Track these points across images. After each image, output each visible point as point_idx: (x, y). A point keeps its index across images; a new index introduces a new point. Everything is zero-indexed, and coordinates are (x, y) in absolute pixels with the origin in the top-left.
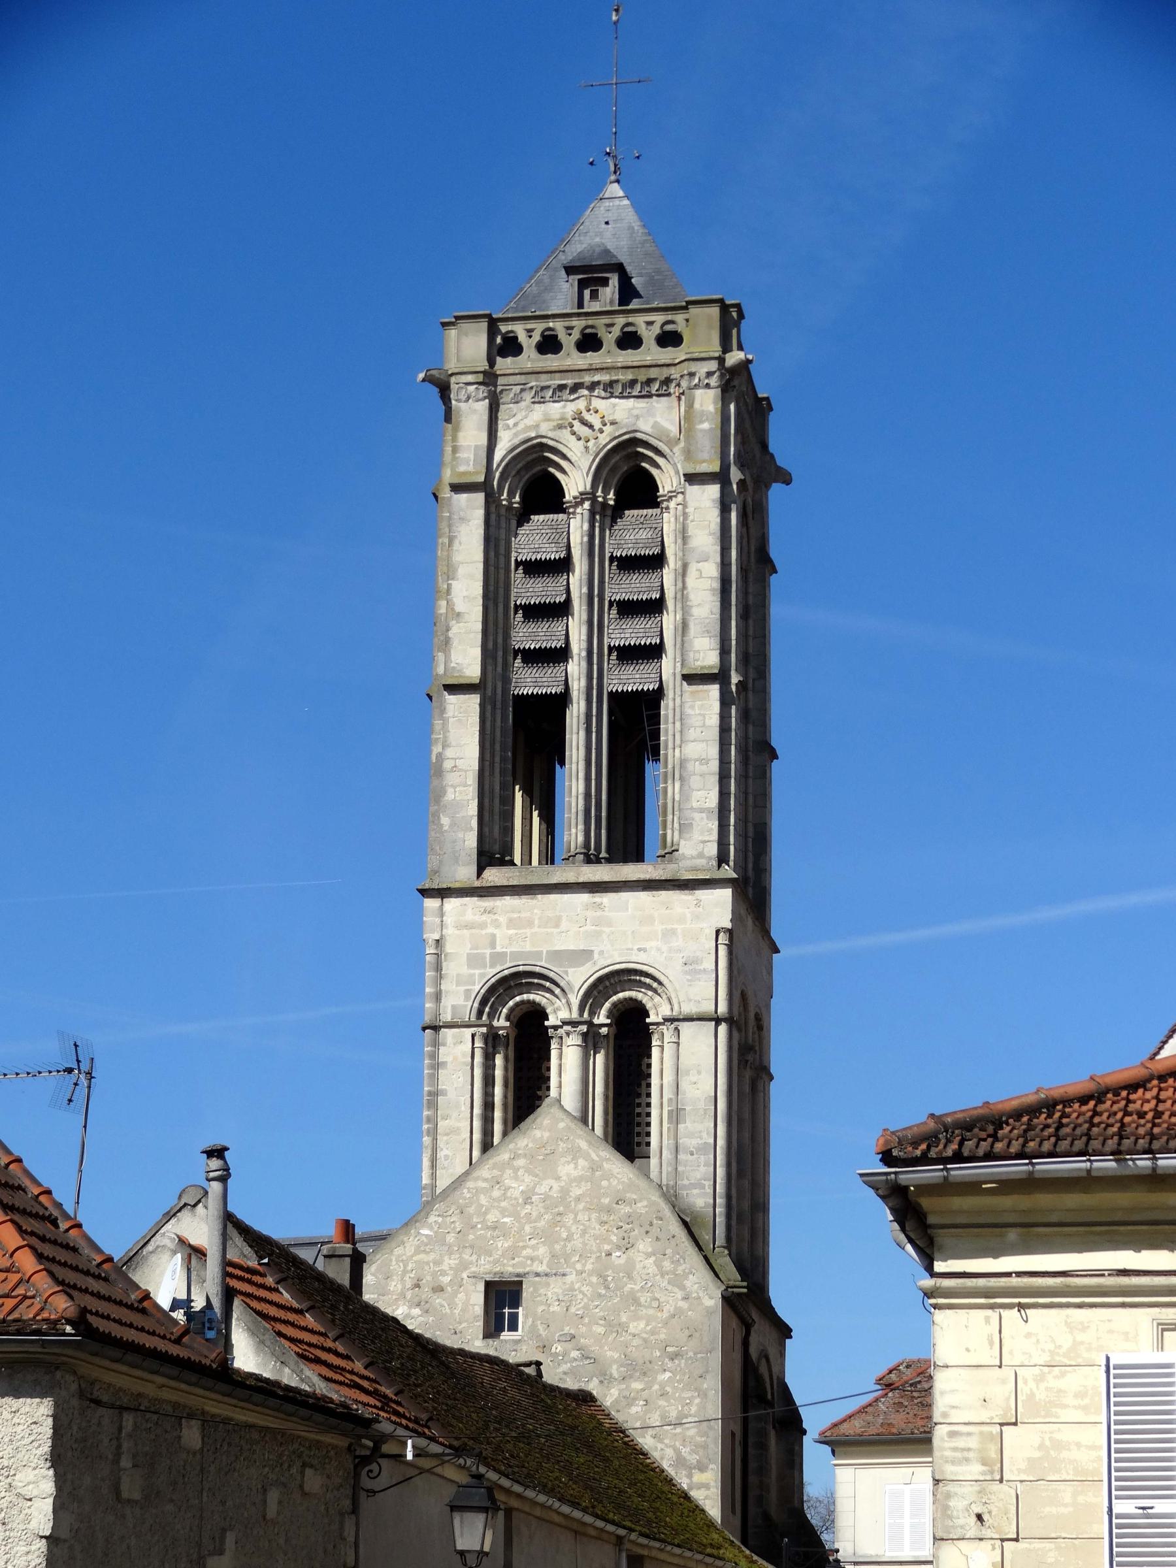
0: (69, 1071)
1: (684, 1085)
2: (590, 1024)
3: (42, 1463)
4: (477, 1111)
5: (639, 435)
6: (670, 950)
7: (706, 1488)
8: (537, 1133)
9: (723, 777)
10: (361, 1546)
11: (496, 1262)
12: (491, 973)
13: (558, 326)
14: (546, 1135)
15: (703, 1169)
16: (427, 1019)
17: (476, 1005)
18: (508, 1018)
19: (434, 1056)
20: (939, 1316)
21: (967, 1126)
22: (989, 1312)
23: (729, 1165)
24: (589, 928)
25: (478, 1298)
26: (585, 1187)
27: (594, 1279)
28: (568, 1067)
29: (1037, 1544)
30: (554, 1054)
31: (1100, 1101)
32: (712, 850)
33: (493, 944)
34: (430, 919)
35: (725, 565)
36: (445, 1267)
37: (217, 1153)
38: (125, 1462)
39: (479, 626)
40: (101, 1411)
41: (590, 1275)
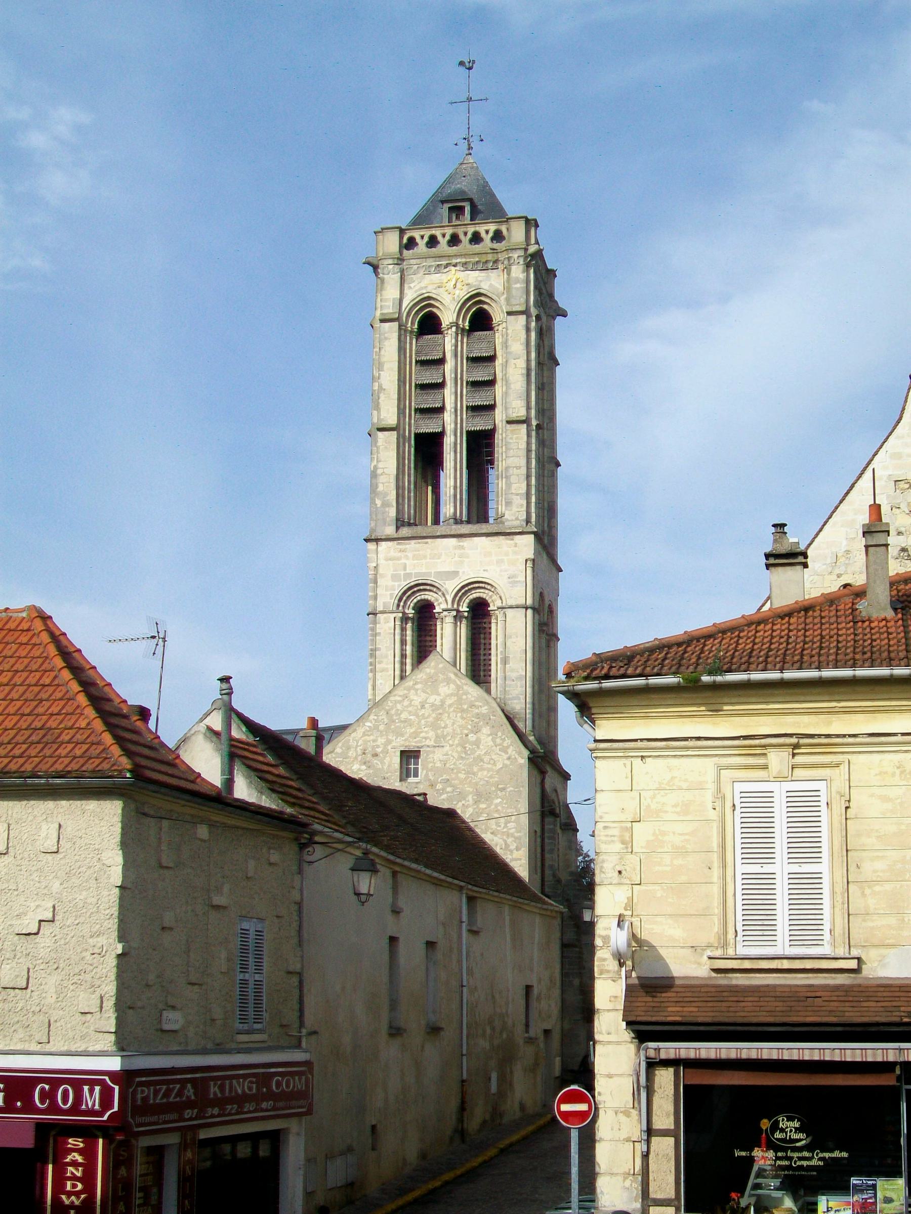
0: (153, 637)
2: (458, 611)
3: (116, 846)
4: (398, 658)
5: (482, 291)
6: (501, 571)
7: (519, 861)
8: (428, 670)
9: (528, 477)
10: (305, 892)
11: (405, 740)
12: (404, 584)
14: (433, 671)
15: (519, 689)
16: (370, 610)
17: (396, 602)
18: (413, 609)
19: (373, 629)
20: (599, 763)
21: (613, 658)
22: (624, 761)
23: (533, 687)
24: (457, 559)
25: (397, 759)
26: (454, 699)
27: (459, 749)
28: (450, 636)
29: (651, 887)
30: (439, 628)
31: (688, 646)
32: (524, 516)
33: (405, 569)
34: (372, 556)
35: (528, 361)
36: (378, 743)
37: (225, 680)
38: (164, 847)
39: (396, 396)
40: (149, 819)
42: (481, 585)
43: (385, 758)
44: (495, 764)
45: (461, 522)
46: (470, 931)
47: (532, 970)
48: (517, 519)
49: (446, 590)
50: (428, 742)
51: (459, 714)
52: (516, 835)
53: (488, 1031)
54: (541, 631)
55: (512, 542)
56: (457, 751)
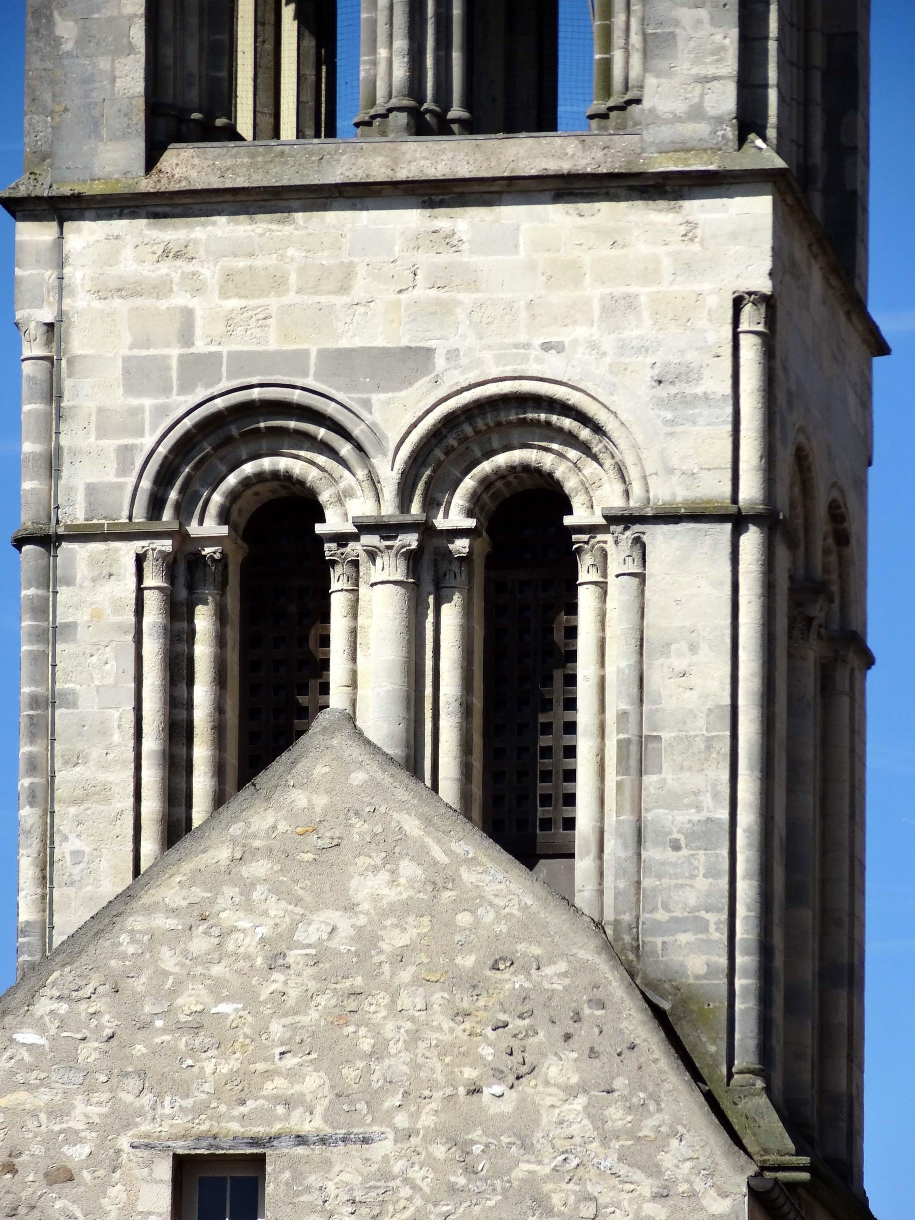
4: (151, 743)
6: (622, 348)
8: (299, 798)
11: (200, 1110)
12: (181, 404)
14: (321, 801)
15: (702, 883)
16: (27, 519)
17: (146, 484)
18: (224, 517)
19: (43, 608)
27: (440, 1151)
28: (372, 635)
30: (338, 604)
33: (186, 336)
34: (30, 273)
36: (76, 1122)
43: (104, 1185)
45: (443, 128)
49: (372, 430)
51: (438, 997)
54: (800, 623)
56: (430, 1162)
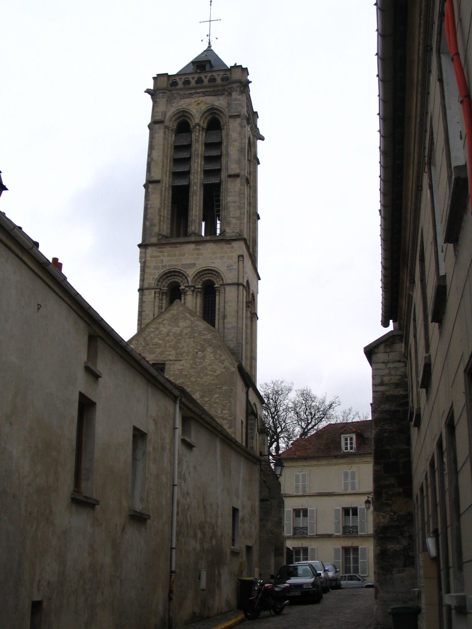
1: (227, 307)
8: (172, 312)
11: (156, 356)
13: (190, 77)
14: (175, 312)
24: (195, 256)
26: (189, 329)
33: (162, 263)
41: (190, 360)
42: (210, 272)
44: (215, 372)
46: (184, 441)
47: (238, 497)
48: (233, 232)
50: (170, 358)
52: (229, 418)
53: (199, 535)
55: (229, 246)
